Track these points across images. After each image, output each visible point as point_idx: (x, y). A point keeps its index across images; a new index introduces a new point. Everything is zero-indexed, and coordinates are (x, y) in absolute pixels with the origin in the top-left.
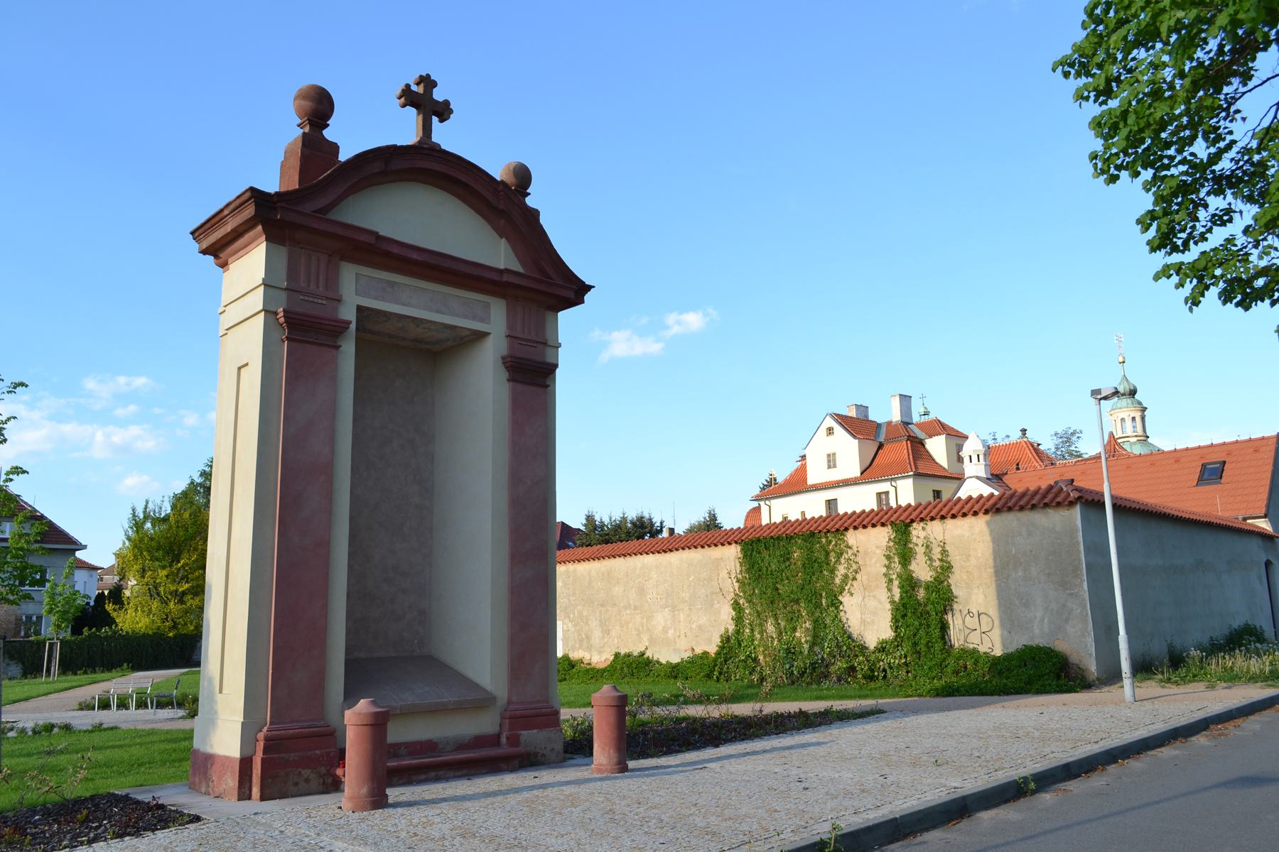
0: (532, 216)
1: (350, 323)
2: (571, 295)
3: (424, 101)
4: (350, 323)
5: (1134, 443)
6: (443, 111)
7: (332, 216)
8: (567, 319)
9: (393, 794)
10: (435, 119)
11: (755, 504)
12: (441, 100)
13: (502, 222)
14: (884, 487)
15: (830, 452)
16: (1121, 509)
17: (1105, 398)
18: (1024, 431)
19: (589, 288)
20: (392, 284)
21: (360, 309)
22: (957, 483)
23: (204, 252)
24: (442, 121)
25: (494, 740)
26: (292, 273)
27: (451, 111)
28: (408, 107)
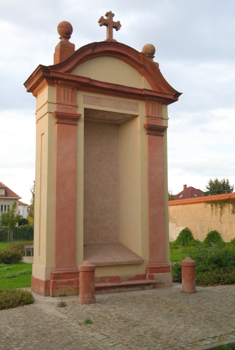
0: (155, 67)
2: (172, 97)
4: (81, 115)
6: (117, 26)
7: (73, 73)
9: (98, 297)
10: (114, 30)
12: (116, 21)
21: (86, 109)
23: (29, 91)
24: (117, 30)
25: (143, 277)
27: (120, 26)
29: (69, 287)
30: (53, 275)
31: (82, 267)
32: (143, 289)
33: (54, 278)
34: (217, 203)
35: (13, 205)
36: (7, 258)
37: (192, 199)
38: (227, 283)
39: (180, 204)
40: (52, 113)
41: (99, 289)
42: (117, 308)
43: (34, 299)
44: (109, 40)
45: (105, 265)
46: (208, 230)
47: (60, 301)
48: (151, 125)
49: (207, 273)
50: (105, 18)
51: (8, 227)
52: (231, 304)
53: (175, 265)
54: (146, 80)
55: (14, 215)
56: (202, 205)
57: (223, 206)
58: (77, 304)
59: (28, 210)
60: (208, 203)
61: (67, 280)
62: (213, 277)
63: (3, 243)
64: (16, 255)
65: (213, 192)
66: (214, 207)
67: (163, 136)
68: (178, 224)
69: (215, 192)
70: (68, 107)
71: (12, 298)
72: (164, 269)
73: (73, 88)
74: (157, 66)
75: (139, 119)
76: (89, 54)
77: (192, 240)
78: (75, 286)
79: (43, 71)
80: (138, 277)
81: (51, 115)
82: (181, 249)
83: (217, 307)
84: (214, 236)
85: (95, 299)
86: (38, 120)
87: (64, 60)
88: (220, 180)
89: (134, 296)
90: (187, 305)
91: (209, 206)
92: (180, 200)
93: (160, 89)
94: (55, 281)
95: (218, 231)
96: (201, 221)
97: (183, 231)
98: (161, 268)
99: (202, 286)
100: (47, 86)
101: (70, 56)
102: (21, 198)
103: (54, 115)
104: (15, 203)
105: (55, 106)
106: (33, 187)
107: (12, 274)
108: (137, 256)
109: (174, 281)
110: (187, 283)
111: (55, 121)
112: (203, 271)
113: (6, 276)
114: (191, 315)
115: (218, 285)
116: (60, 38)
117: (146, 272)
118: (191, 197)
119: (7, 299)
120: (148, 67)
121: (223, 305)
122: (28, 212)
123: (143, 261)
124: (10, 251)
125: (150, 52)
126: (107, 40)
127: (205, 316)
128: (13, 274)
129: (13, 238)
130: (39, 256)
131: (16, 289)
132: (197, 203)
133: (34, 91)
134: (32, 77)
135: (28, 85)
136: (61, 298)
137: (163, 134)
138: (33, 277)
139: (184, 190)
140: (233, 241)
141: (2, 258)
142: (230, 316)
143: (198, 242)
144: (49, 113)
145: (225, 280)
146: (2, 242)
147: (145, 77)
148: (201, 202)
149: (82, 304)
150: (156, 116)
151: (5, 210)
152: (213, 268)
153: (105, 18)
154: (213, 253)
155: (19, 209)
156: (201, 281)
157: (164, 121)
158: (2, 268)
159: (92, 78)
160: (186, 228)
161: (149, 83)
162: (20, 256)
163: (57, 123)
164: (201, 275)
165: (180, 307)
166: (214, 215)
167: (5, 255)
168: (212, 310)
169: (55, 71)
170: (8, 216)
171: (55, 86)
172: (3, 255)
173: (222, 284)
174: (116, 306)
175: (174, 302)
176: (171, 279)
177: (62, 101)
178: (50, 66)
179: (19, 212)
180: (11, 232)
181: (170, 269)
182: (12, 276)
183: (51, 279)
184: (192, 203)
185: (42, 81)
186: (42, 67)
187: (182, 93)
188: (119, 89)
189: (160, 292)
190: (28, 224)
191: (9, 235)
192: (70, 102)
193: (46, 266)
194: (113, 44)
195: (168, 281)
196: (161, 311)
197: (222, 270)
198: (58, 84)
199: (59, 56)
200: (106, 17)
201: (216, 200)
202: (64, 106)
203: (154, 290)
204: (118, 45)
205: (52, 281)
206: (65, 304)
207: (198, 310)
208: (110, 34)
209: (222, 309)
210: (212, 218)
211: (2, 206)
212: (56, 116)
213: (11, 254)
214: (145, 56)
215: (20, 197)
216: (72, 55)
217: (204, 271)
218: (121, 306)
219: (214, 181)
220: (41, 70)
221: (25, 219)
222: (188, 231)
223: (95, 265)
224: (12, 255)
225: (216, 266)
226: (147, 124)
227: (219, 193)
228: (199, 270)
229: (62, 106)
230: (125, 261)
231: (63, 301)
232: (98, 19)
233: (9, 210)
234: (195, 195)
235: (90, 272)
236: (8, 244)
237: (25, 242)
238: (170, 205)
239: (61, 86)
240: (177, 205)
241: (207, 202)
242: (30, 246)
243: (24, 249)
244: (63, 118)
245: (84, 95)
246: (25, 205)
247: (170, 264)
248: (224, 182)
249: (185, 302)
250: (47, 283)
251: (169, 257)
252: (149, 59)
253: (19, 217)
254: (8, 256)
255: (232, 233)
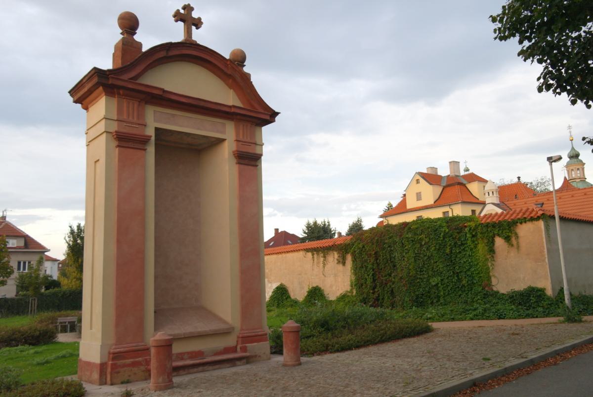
0: (247, 77)
1: (151, 137)
2: (268, 118)
3: (186, 17)
4: (151, 137)
5: (579, 182)
6: (198, 23)
8: (267, 131)
9: (176, 380)
10: (194, 28)
11: (381, 219)
12: (196, 17)
13: (231, 81)
14: (446, 209)
15: (418, 191)
16: (562, 219)
17: (555, 161)
18: (519, 178)
19: (277, 114)
20: (173, 115)
21: (157, 129)
22: (482, 206)
23: (76, 102)
24: (197, 28)
25: (233, 350)
26: (120, 111)
27: (202, 23)
28: (179, 22)
29: (135, 369)
30: (111, 355)
31: (155, 340)
32: (234, 365)
33: (113, 359)
34: (319, 251)
35: (38, 261)
36: (33, 337)
37: (286, 247)
38: (338, 351)
39: (274, 254)
40: (111, 133)
41: (177, 370)
42: (203, 393)
43: (85, 389)
44: (188, 41)
45: (183, 337)
46: (309, 286)
47: (124, 390)
48: (242, 152)
49: (313, 339)
50: (182, 11)
51: (30, 293)
52: (345, 375)
53: (272, 332)
54: (234, 93)
55: (39, 274)
56: (301, 253)
57: (327, 254)
58: (148, 392)
59: (59, 267)
60: (308, 252)
61: (132, 360)
62: (319, 344)
63: (21, 317)
64: (47, 332)
65: (312, 238)
66: (315, 256)
67: (257, 166)
68: (270, 280)
69: (314, 237)
70: (133, 125)
71: (53, 391)
72: (259, 338)
73: (139, 100)
74: (248, 77)
75: (226, 144)
76: (162, 58)
77: (289, 300)
78: (143, 368)
79: (99, 76)
80: (227, 350)
81: (110, 136)
82: (276, 311)
83: (328, 381)
84: (316, 293)
85: (173, 383)
86: (89, 142)
87: (129, 63)
88: (320, 222)
89: (224, 376)
90: (292, 381)
91: (310, 254)
92: (271, 249)
93: (252, 106)
94: (114, 362)
95: (321, 286)
96: (300, 274)
97: (277, 288)
98: (256, 336)
99: (306, 356)
100: (104, 97)
101: (136, 58)
102: (49, 251)
103: (113, 136)
104: (42, 258)
105: (116, 123)
106: (68, 234)
107: (44, 359)
108: (225, 322)
109: (271, 353)
110: (290, 353)
111: (116, 143)
112: (306, 337)
113: (35, 362)
114: (298, 393)
115: (326, 354)
116: (121, 34)
117: (237, 343)
118: (284, 245)
119: (44, 392)
120: (239, 79)
121: (335, 377)
122: (59, 270)
123: (233, 328)
124: (38, 327)
125: (239, 59)
126: (185, 40)
127: (316, 393)
128: (46, 359)
129: (37, 309)
130: (91, 329)
131: (56, 379)
132: (294, 251)
133: (83, 103)
134: (82, 83)
135: (76, 94)
136: (125, 385)
137: (257, 164)
138: (81, 360)
139: (275, 236)
140: (339, 298)
141: (25, 337)
142: (345, 389)
143: (296, 302)
144: (107, 132)
145: (335, 346)
146: (20, 315)
147: (234, 89)
148: (299, 250)
149: (155, 391)
150: (248, 140)
151: (24, 269)
152: (320, 333)
153: (182, 11)
154: (318, 314)
155: (46, 266)
156: (306, 350)
157: (258, 147)
158: (27, 352)
159: (166, 89)
160: (281, 285)
161: (239, 98)
162: (53, 333)
163: (118, 146)
164: (305, 343)
165: (284, 384)
166: (315, 266)
167: (30, 333)
168: (323, 384)
169: (115, 77)
170: (31, 277)
171: (115, 97)
172: (27, 332)
173: (331, 353)
174: (202, 390)
175: (276, 378)
176: (268, 351)
177: (125, 117)
178: (109, 70)
179: (46, 270)
180: (35, 299)
181: (267, 337)
182: (44, 361)
183: (109, 360)
184: (288, 252)
185: (97, 88)
186: (97, 71)
187: (280, 113)
188: (202, 104)
189: (256, 368)
190: (60, 287)
191: (32, 305)
192: (135, 119)
193: (102, 343)
194: (193, 46)
195: (264, 353)
196: (261, 391)
197: (330, 334)
198: (119, 94)
199: (120, 58)
200: (183, 10)
201: (318, 248)
202: (128, 125)
203: (248, 366)
204: (200, 47)
205: (111, 362)
206: (132, 393)
207: (306, 386)
208: (189, 33)
209: (335, 382)
210: (313, 270)
211: (19, 263)
212: (117, 137)
213: (40, 331)
214: (234, 64)
215: (47, 249)
216: (140, 57)
217: (308, 337)
218: (208, 389)
219: (312, 222)
220: (96, 74)
221: (54, 281)
222: (284, 288)
223: (172, 337)
224: (42, 332)
225: (323, 329)
226: (237, 151)
227: (319, 238)
228: (302, 337)
229: (125, 124)
230: (210, 330)
231: (129, 389)
232: (173, 13)
233: (30, 268)
234: (290, 242)
235: (166, 346)
236: (30, 316)
237: (58, 313)
238: (267, 255)
239: (123, 97)
240: (269, 254)
241: (307, 250)
242: (66, 318)
243: (56, 323)
244: (126, 141)
245: (154, 111)
246: (55, 260)
247: (269, 331)
248: (325, 225)
249: (289, 377)
250: (103, 366)
251: (265, 323)
252: (240, 68)
253: (46, 277)
254: (35, 334)
255: (338, 288)
